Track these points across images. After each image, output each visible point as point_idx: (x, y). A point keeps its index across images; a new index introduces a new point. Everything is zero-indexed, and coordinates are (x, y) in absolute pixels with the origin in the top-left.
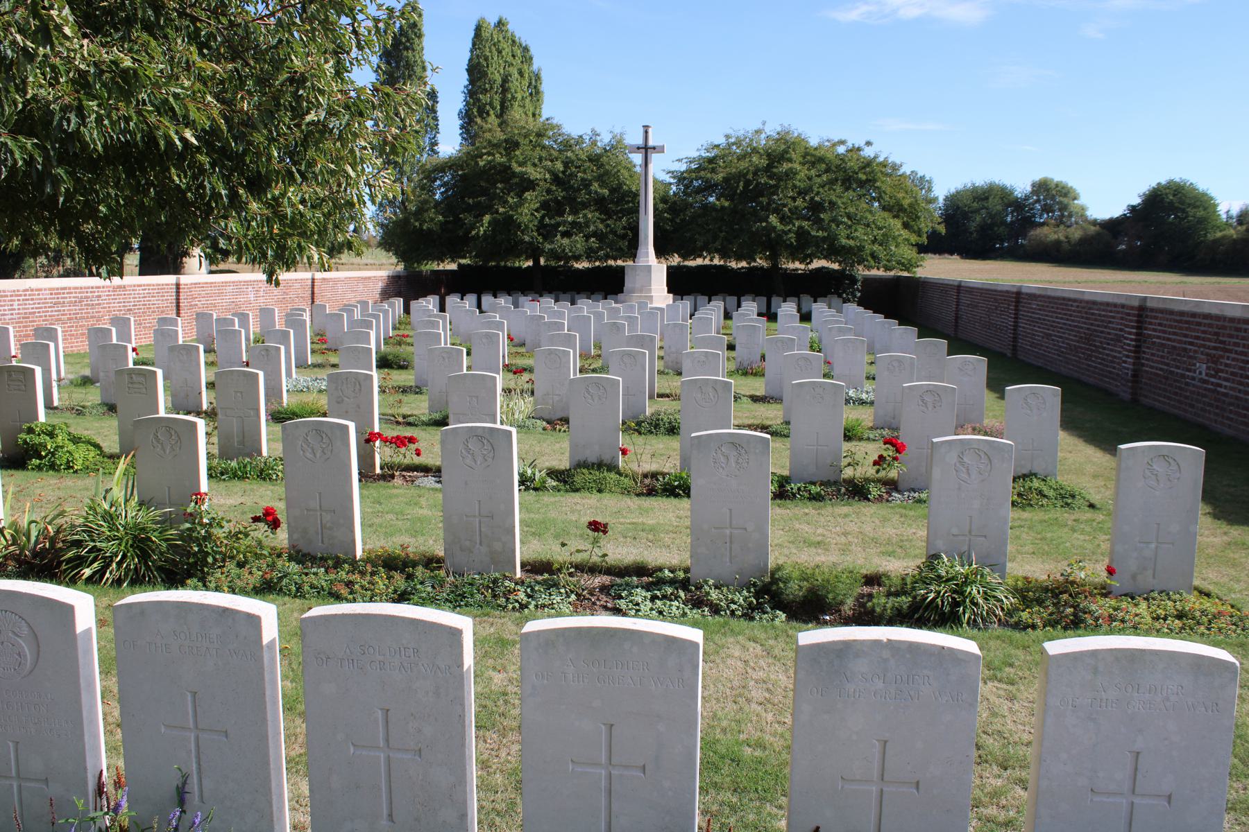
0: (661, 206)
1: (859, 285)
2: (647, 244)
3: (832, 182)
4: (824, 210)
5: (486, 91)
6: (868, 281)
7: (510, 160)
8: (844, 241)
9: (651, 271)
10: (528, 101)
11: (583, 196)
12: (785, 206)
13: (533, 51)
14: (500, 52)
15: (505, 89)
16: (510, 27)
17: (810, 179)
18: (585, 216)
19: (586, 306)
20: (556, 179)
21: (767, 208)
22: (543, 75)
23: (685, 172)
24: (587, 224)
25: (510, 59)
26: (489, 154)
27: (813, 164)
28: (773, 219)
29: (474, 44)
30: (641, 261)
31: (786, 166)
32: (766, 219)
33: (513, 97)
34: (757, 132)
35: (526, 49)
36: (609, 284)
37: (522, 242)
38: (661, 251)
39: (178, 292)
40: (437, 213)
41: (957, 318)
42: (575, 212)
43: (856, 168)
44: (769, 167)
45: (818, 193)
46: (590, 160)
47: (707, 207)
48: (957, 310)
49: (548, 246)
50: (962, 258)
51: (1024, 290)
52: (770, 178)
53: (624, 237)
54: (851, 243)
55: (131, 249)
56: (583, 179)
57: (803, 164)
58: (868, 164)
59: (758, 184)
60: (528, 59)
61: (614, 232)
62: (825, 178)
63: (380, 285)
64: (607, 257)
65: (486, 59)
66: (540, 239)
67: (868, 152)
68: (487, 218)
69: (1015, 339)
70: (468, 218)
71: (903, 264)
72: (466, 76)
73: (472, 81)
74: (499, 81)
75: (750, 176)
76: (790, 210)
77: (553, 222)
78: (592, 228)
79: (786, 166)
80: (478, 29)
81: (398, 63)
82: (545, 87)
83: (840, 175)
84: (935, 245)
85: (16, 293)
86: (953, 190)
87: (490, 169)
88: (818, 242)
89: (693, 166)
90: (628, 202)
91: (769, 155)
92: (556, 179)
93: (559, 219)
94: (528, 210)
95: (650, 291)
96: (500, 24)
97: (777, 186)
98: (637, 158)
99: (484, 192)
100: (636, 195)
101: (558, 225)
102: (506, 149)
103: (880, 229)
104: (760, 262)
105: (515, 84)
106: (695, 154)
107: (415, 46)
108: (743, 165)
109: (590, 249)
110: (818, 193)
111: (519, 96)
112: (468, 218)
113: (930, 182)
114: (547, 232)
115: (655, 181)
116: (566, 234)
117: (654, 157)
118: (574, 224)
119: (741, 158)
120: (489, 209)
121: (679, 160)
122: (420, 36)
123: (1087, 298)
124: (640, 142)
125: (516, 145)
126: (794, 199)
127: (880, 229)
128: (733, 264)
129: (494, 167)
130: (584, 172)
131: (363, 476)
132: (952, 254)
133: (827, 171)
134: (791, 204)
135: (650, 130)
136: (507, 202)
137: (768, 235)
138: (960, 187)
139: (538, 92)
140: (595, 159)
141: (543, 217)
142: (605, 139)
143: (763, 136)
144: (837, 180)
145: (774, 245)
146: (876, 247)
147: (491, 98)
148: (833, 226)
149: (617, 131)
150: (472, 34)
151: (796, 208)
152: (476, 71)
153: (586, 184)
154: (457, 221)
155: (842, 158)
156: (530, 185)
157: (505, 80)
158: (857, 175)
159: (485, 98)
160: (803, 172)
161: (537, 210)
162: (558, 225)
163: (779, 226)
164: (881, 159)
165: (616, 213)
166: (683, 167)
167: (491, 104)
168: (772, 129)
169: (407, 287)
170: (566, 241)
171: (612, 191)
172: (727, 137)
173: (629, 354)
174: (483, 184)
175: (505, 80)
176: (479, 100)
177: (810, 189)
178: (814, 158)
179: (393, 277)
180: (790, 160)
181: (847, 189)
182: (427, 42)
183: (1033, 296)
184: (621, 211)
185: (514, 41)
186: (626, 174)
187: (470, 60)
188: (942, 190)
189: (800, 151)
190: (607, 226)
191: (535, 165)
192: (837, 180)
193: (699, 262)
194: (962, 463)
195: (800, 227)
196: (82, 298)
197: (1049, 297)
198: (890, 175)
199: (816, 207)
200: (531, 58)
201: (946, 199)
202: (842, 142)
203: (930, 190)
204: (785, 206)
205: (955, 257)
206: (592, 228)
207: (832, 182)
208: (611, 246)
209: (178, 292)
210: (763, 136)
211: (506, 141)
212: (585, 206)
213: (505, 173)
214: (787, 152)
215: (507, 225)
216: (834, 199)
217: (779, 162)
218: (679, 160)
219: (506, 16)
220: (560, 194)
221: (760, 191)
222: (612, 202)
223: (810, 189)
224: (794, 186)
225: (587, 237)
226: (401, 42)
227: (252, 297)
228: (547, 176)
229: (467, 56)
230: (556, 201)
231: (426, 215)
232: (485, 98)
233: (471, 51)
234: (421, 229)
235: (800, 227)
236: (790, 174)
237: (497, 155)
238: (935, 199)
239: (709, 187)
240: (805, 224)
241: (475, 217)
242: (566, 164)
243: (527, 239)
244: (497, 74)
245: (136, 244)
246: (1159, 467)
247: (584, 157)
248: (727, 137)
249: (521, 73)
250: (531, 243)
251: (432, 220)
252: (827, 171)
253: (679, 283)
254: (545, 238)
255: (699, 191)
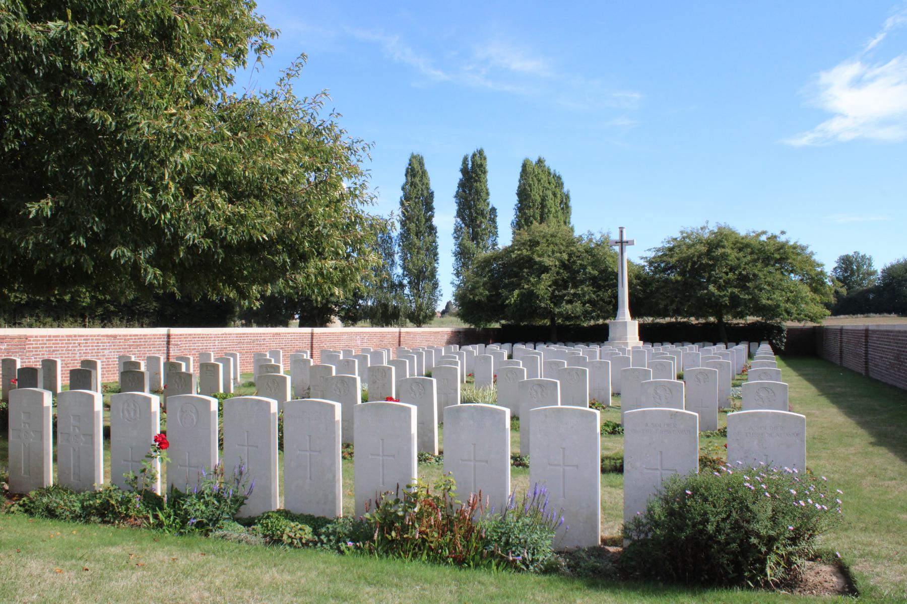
0: (635, 281)
1: (785, 334)
2: (624, 307)
3: (755, 261)
4: (749, 280)
5: (530, 207)
6: (791, 331)
7: (533, 253)
8: (764, 301)
9: (626, 327)
10: (560, 213)
11: (581, 276)
12: (721, 278)
13: (564, 179)
14: (539, 181)
15: (543, 206)
16: (546, 164)
17: (738, 259)
18: (582, 289)
19: (580, 350)
20: (564, 265)
21: (709, 281)
22: (571, 195)
23: (654, 258)
24: (584, 296)
25: (547, 185)
26: (518, 250)
27: (740, 250)
28: (712, 288)
29: (521, 176)
30: (620, 319)
31: (720, 251)
32: (707, 288)
33: (549, 211)
34: (702, 229)
35: (559, 178)
36: (600, 335)
37: (540, 307)
38: (634, 314)
39: (312, 338)
40: (485, 289)
41: (841, 352)
42: (575, 286)
43: (772, 251)
44: (709, 251)
45: (744, 269)
46: (587, 252)
47: (667, 281)
48: (841, 347)
49: (557, 310)
50: (899, 315)
51: (870, 328)
52: (710, 259)
53: (609, 303)
54: (770, 302)
55: (293, 318)
56: (581, 265)
57: (732, 249)
58: (782, 246)
59: (702, 264)
60: (559, 183)
61: (603, 300)
62: (749, 258)
63: (446, 337)
64: (598, 317)
65: (530, 186)
66: (552, 305)
67: (782, 239)
68: (516, 292)
69: (866, 363)
70: (504, 292)
71: (809, 317)
72: (516, 198)
73: (520, 202)
74: (539, 200)
75: (695, 259)
76: (724, 281)
77: (560, 293)
78: (587, 297)
79: (720, 251)
80: (524, 166)
81: (470, 190)
82: (573, 203)
83: (762, 256)
84: (843, 307)
85: (217, 336)
86: (888, 265)
87: (520, 259)
88: (745, 303)
89: (660, 254)
90: (612, 280)
91: (708, 244)
92: (564, 265)
93: (564, 292)
94: (543, 286)
95: (626, 339)
96: (540, 162)
97: (714, 265)
98: (617, 248)
99: (516, 275)
100: (616, 275)
101: (564, 295)
102: (530, 246)
103: (792, 292)
104: (712, 319)
105: (550, 202)
106: (660, 245)
107: (482, 179)
108: (692, 251)
109: (586, 311)
110: (744, 269)
111: (553, 210)
112: (504, 292)
113: (870, 259)
114: (557, 300)
115: (629, 262)
116: (570, 302)
117: (628, 249)
118: (575, 295)
119: (689, 247)
120: (518, 286)
121: (649, 250)
122: (485, 172)
123: (897, 329)
124: (617, 238)
125: (538, 243)
126: (727, 273)
127: (792, 292)
128: (693, 320)
129: (523, 258)
130: (582, 260)
131: (422, 459)
132: (890, 313)
133: (751, 253)
134: (725, 277)
135: (624, 230)
136: (529, 281)
137: (709, 299)
138: (894, 262)
139: (567, 207)
140: (589, 251)
141: (554, 291)
142: (597, 237)
143: (707, 231)
144: (758, 259)
145: (717, 308)
146: (788, 305)
147: (534, 212)
148: (756, 291)
149: (605, 231)
150: (520, 169)
151: (729, 279)
152: (523, 194)
153: (584, 267)
154: (499, 295)
155: (762, 244)
156: (546, 269)
157: (543, 199)
158: (778, 256)
159: (529, 212)
160: (733, 254)
161: (550, 286)
162: (564, 295)
163: (716, 292)
164: (791, 243)
165: (604, 287)
166: (651, 255)
167: (534, 216)
168: (713, 227)
169: (462, 338)
170: (569, 306)
171: (601, 272)
172: (682, 232)
173: (555, 363)
174: (515, 269)
175: (543, 199)
176: (525, 213)
177: (738, 266)
178: (742, 245)
179: (455, 332)
180: (724, 247)
181: (767, 265)
182: (489, 176)
183: (874, 331)
184: (608, 285)
185: (549, 173)
186: (611, 260)
187: (519, 187)
188: (879, 265)
189: (732, 240)
190: (598, 296)
191: (549, 256)
192: (758, 259)
193: (668, 320)
194: (656, 393)
195: (732, 293)
196: (255, 339)
197: (881, 331)
198: (798, 254)
199: (743, 280)
200: (562, 184)
201: (883, 271)
202: (764, 233)
203: (870, 265)
204: (721, 278)
205: (893, 315)
206: (587, 297)
207: (755, 261)
208: (600, 309)
209: (312, 338)
210: (707, 231)
211: (530, 240)
212: (582, 282)
213: (528, 262)
214: (721, 241)
215: (530, 296)
216: (756, 272)
217: (716, 248)
218: (649, 250)
219: (543, 156)
220: (566, 275)
221: (705, 267)
222: (601, 279)
223: (738, 266)
224: (727, 264)
225: (584, 304)
226: (472, 177)
227: (359, 342)
228: (557, 263)
229: (516, 184)
230: (563, 280)
231: (477, 291)
232: (529, 212)
233: (520, 181)
234: (474, 300)
235: (732, 293)
236: (724, 256)
237: (524, 251)
238: (875, 272)
239: (670, 268)
240: (736, 290)
241: (509, 291)
242: (570, 255)
243: (543, 305)
244: (540, 195)
245: (297, 316)
246: (763, 394)
247: (581, 250)
248: (682, 232)
249: (555, 194)
250: (546, 308)
251: (481, 294)
252: (751, 253)
253: (648, 335)
254: (555, 305)
255: (664, 270)
